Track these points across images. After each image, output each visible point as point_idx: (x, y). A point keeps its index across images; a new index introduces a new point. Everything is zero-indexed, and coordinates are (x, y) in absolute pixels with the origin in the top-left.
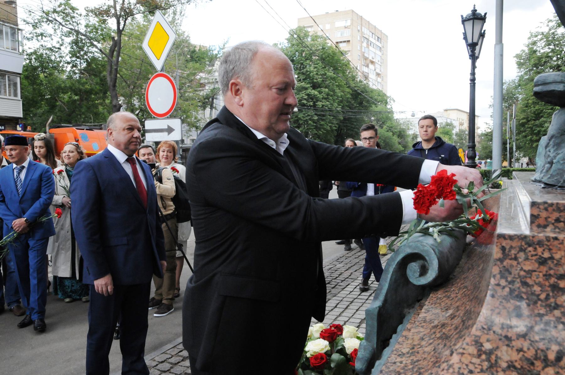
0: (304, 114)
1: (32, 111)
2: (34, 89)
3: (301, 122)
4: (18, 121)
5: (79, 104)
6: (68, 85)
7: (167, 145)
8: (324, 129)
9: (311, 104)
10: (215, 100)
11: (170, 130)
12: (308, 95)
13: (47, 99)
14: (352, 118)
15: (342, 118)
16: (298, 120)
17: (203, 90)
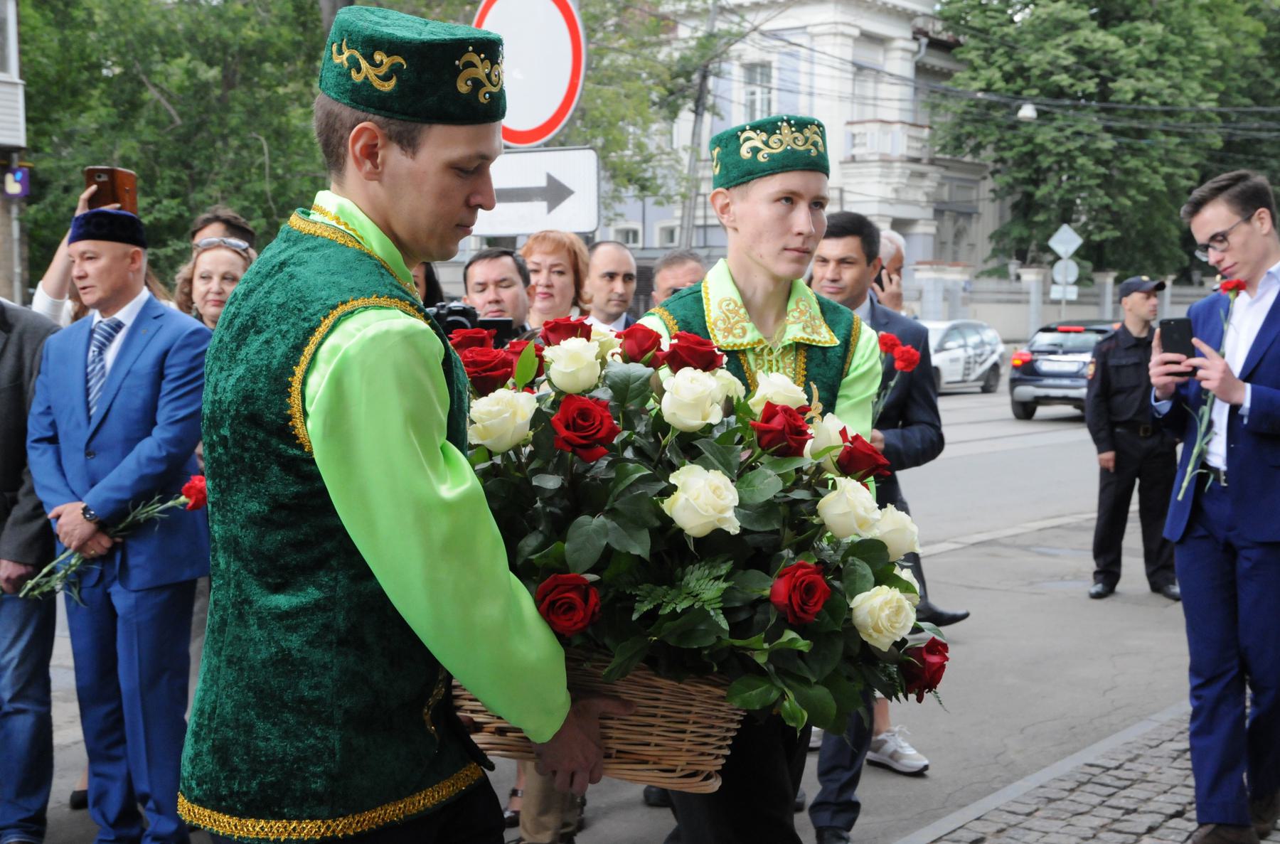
0: (1061, 130)
1: (58, 121)
2: (64, 44)
3: (1045, 161)
4: (9, 159)
5: (219, 99)
6: (179, 27)
7: (548, 247)
8: (1141, 188)
9: (1091, 86)
10: (711, 82)
11: (555, 193)
12: (1079, 52)
13: (108, 80)
14: (1260, 141)
15: (1218, 143)
16: (1032, 155)
17: (668, 42)
